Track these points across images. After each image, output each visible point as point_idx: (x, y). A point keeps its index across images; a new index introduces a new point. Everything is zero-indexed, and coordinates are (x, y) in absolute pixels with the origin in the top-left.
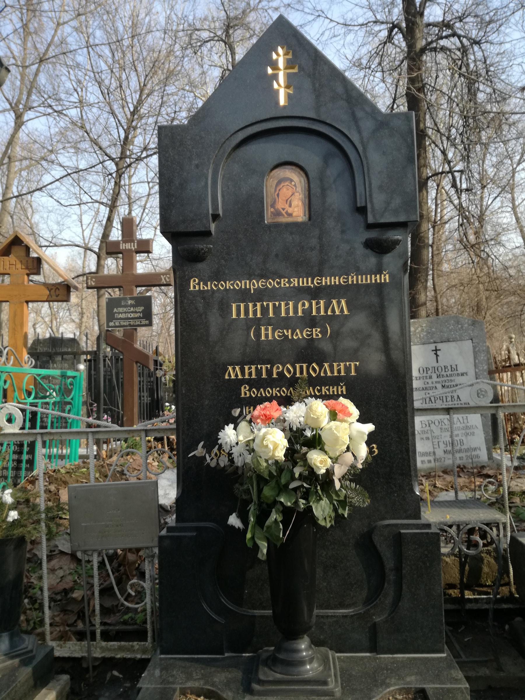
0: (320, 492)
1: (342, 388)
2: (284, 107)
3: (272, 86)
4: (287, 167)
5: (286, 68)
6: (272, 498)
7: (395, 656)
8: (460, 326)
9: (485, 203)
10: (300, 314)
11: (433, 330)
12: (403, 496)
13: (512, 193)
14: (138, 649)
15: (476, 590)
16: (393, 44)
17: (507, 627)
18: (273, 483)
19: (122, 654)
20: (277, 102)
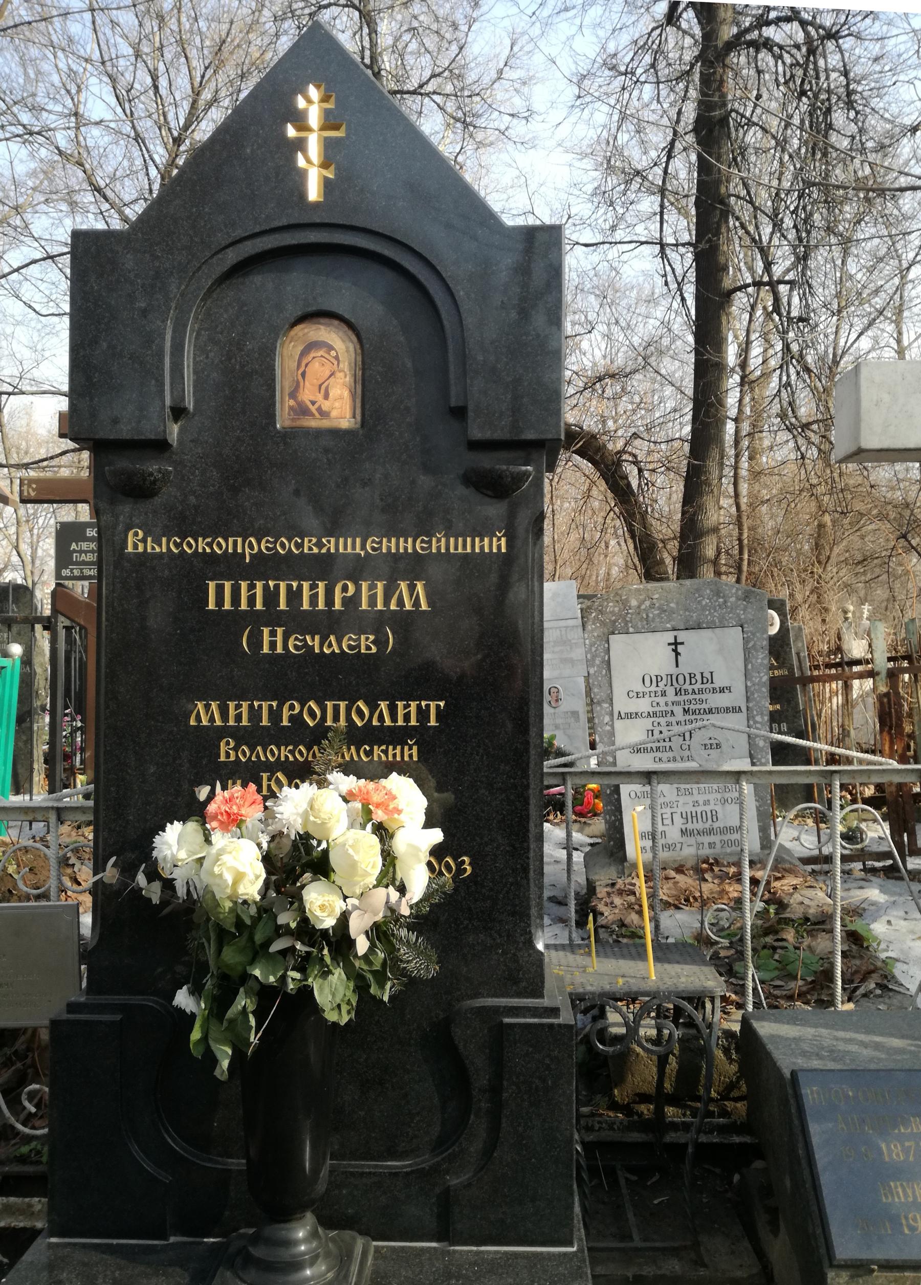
0: (328, 959)
1: (411, 749)
2: (316, 205)
3: (294, 160)
4: (322, 320)
5: (323, 128)
6: (240, 968)
7: (483, 1248)
8: (721, 600)
9: (842, 342)
10: (338, 606)
11: (672, 605)
12: (514, 955)
13: (898, 323)
14: (39, 1211)
15: (690, 1107)
16: (679, 28)
17: (736, 1178)
18: (243, 941)
19: (9, 1221)
20: (303, 195)
